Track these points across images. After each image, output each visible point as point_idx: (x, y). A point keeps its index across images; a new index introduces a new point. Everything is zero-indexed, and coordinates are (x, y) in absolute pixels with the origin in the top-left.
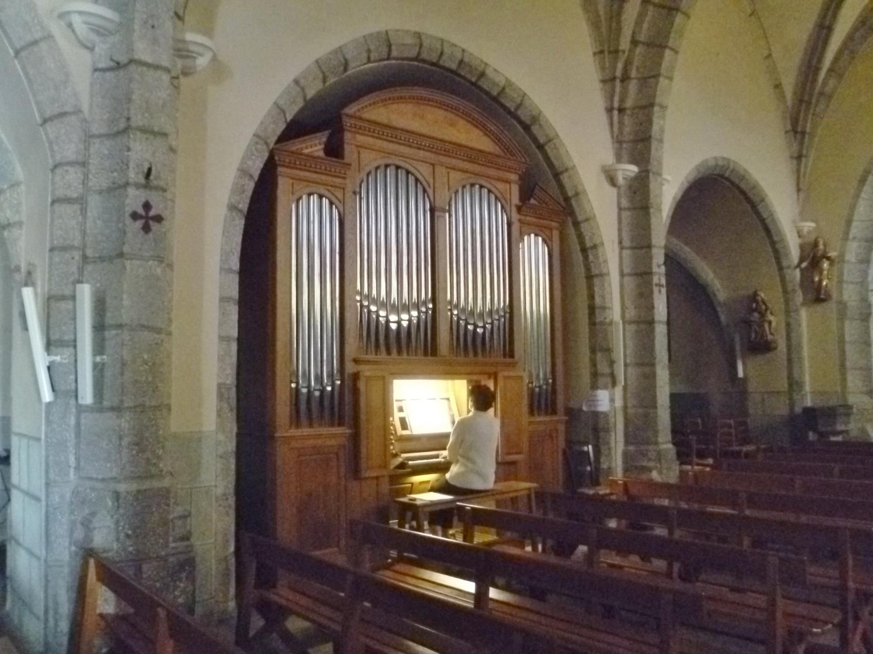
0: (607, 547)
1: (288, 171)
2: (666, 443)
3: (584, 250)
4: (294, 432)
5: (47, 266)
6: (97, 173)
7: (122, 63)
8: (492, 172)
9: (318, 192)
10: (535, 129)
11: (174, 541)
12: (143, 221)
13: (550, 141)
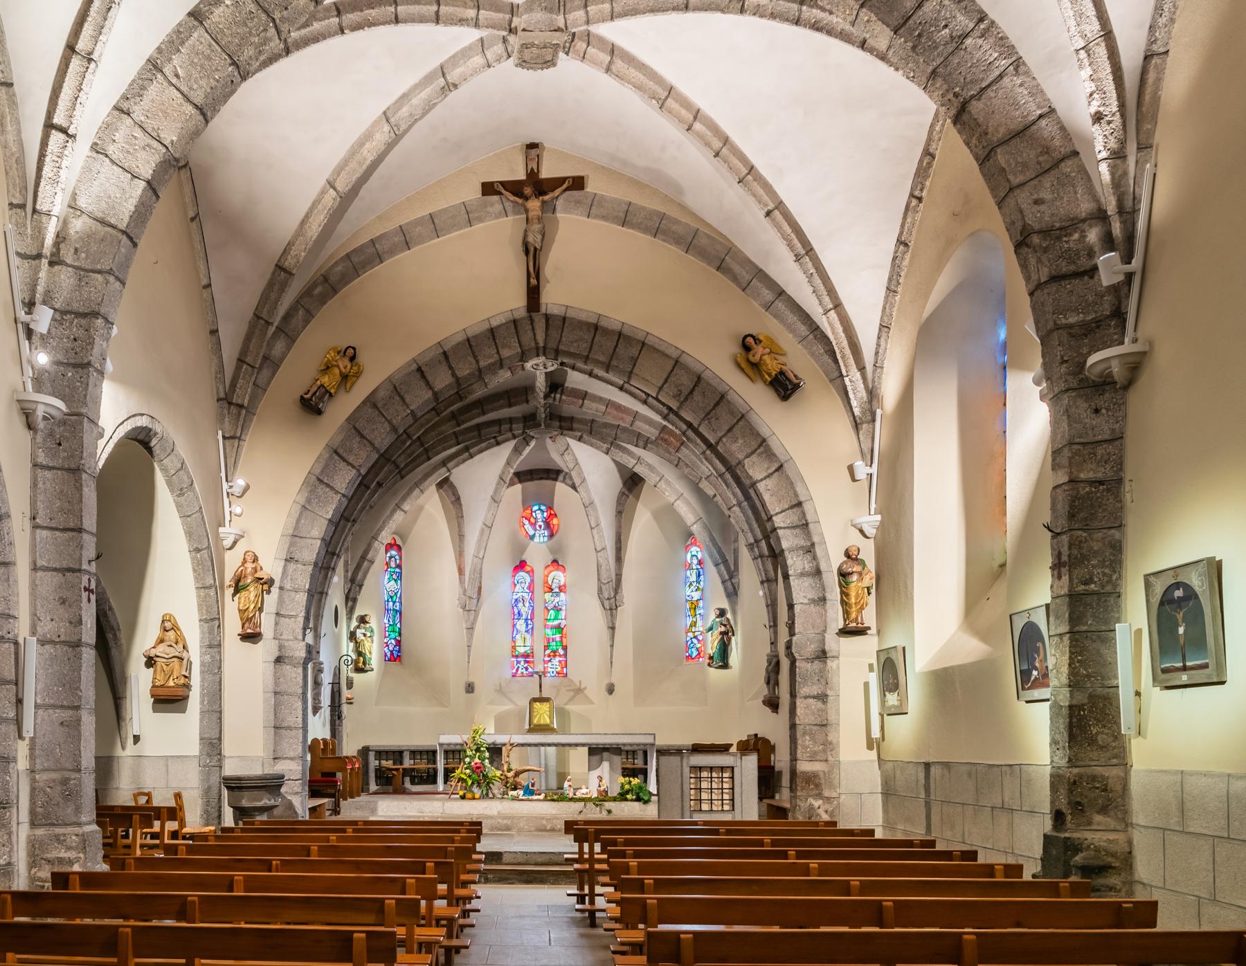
2: (89, 823)
5: (809, 357)
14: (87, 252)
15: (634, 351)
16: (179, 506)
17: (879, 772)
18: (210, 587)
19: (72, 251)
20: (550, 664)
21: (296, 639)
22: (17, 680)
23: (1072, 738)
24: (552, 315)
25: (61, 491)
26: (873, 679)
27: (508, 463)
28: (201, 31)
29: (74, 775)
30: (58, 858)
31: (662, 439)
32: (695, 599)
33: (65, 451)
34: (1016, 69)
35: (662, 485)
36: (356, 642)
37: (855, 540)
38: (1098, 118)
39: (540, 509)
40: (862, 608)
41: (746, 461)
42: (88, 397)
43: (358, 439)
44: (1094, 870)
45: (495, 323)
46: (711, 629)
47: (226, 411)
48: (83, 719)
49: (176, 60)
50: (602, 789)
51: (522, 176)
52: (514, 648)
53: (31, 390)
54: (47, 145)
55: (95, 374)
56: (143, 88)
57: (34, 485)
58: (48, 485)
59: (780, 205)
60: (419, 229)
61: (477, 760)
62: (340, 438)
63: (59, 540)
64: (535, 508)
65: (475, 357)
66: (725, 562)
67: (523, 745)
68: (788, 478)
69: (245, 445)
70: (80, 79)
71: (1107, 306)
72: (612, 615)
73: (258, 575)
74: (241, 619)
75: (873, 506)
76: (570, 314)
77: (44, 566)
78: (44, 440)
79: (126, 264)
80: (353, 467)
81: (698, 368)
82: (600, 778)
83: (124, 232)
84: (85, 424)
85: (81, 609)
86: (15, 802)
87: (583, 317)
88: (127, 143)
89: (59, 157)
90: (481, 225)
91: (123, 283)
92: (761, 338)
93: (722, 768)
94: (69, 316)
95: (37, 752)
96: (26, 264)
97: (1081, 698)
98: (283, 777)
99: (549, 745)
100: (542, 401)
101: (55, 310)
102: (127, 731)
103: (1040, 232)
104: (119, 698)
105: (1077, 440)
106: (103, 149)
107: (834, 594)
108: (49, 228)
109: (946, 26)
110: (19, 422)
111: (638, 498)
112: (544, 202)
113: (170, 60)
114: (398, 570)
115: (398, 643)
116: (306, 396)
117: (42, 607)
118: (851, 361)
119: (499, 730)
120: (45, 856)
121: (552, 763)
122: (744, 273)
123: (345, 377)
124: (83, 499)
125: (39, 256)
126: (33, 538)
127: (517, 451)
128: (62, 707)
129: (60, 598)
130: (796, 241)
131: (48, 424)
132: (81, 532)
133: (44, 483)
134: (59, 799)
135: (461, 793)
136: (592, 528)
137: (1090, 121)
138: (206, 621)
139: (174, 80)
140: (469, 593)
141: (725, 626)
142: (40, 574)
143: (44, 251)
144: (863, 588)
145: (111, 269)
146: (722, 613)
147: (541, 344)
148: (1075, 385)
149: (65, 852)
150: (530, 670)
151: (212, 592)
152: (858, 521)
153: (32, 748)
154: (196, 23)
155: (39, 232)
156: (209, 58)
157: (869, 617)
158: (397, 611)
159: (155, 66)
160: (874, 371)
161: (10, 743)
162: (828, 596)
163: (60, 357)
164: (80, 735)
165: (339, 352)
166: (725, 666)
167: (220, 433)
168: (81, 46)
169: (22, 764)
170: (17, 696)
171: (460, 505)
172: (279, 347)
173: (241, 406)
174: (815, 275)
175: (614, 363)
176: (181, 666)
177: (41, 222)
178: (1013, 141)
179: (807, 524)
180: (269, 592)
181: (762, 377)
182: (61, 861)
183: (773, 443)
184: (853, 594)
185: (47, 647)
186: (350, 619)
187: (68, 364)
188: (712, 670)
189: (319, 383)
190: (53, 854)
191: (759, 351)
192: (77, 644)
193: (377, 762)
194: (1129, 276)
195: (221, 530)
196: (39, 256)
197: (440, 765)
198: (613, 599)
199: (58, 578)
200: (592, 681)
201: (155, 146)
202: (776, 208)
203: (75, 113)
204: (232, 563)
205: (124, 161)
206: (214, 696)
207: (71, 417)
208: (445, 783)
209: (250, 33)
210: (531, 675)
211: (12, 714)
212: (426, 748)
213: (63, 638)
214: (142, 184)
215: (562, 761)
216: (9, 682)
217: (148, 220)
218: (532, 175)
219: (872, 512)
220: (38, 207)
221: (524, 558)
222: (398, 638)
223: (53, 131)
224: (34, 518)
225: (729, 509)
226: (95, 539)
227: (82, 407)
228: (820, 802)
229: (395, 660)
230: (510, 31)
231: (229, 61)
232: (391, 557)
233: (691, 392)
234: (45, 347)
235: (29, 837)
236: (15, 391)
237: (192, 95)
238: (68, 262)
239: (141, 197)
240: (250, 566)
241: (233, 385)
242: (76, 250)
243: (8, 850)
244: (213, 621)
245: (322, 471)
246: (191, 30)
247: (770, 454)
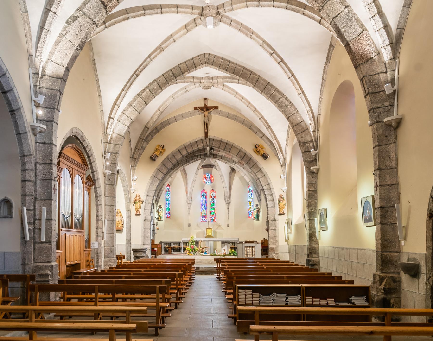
0: (49, 299)
3: (96, 196)
6: (39, 174)
7: (46, 143)
10: (91, 158)
14: (116, 141)
15: (230, 147)
16: (123, 184)
17: (288, 247)
18: (128, 203)
20: (211, 218)
21: (149, 215)
23: (309, 240)
24: (211, 138)
25: (110, 189)
26: (286, 225)
27: (200, 165)
28: (140, 98)
29: (113, 247)
31: (239, 162)
32: (251, 201)
33: (111, 181)
34: (297, 113)
35: (241, 172)
36: (158, 213)
37: (282, 193)
38: (310, 124)
39: (208, 175)
40: (283, 209)
41: (257, 173)
43: (164, 167)
44: (313, 265)
45: (197, 140)
46: (254, 210)
47: (132, 160)
49: (134, 103)
50: (225, 252)
51: (203, 106)
52: (201, 214)
56: (128, 109)
57: (105, 188)
59: (262, 117)
60: (179, 117)
61: (192, 245)
62: (160, 167)
64: (207, 175)
65: (192, 147)
66: (258, 192)
67: (204, 241)
68: (266, 178)
69: (136, 168)
71: (314, 158)
72: (228, 205)
73: (140, 200)
74: (136, 210)
75: (286, 185)
76: (215, 138)
80: (163, 173)
81: (245, 152)
82: (224, 250)
83: (123, 137)
87: (218, 139)
90: (194, 117)
92: (260, 145)
93: (252, 247)
97: (311, 232)
98: (147, 249)
99: (211, 241)
100: (209, 152)
103: (302, 143)
105: (310, 183)
107: (277, 205)
109: (284, 103)
110: (103, 175)
111: (235, 173)
112: (208, 112)
113: (133, 103)
114: (169, 192)
115: (169, 213)
116: (152, 157)
118: (280, 152)
119: (197, 237)
121: (212, 246)
122: (255, 130)
123: (161, 152)
126: (105, 199)
127: (202, 161)
128: (110, 233)
130: (266, 125)
135: (188, 254)
136: (222, 182)
137: (309, 124)
138: (128, 211)
139: (134, 107)
140: (189, 199)
141: (258, 209)
142: (106, 206)
144: (283, 204)
146: (257, 205)
147: (208, 145)
148: (309, 172)
150: (206, 220)
151: (129, 204)
152: (282, 188)
153: (105, 242)
154: (139, 96)
156: (141, 102)
157: (285, 211)
158: (169, 204)
159: (130, 105)
160: (285, 154)
162: (276, 206)
165: (159, 146)
166: (258, 220)
167: (131, 165)
169: (103, 245)
171: (186, 174)
172: (145, 144)
173: (136, 159)
174: (271, 132)
175: (225, 149)
176: (122, 222)
178: (297, 125)
179: (271, 189)
180: (142, 204)
181: (260, 154)
182: (110, 265)
183: (263, 170)
184: (281, 206)
186: (157, 206)
187: (112, 163)
188: (255, 221)
189: (155, 154)
190: (109, 264)
191: (259, 148)
193: (164, 246)
194: (394, 91)
195: (131, 189)
196: (107, 142)
197: (182, 246)
198: (228, 201)
200: (223, 224)
202: (262, 117)
204: (133, 197)
206: (129, 229)
208: (183, 251)
209: (149, 98)
210: (206, 221)
211: (102, 235)
212: (167, 242)
213: (110, 219)
214: (127, 127)
215: (215, 246)
218: (206, 106)
219: (286, 186)
220: (107, 133)
221: (204, 189)
222: (169, 211)
225: (257, 180)
228: (275, 255)
229: (168, 217)
230: (201, 83)
231: (145, 103)
232: (167, 189)
233: (244, 157)
235: (104, 260)
237: (137, 110)
240: (138, 198)
241: (134, 153)
244: (129, 211)
245: (155, 175)
246: (137, 98)
247: (262, 172)
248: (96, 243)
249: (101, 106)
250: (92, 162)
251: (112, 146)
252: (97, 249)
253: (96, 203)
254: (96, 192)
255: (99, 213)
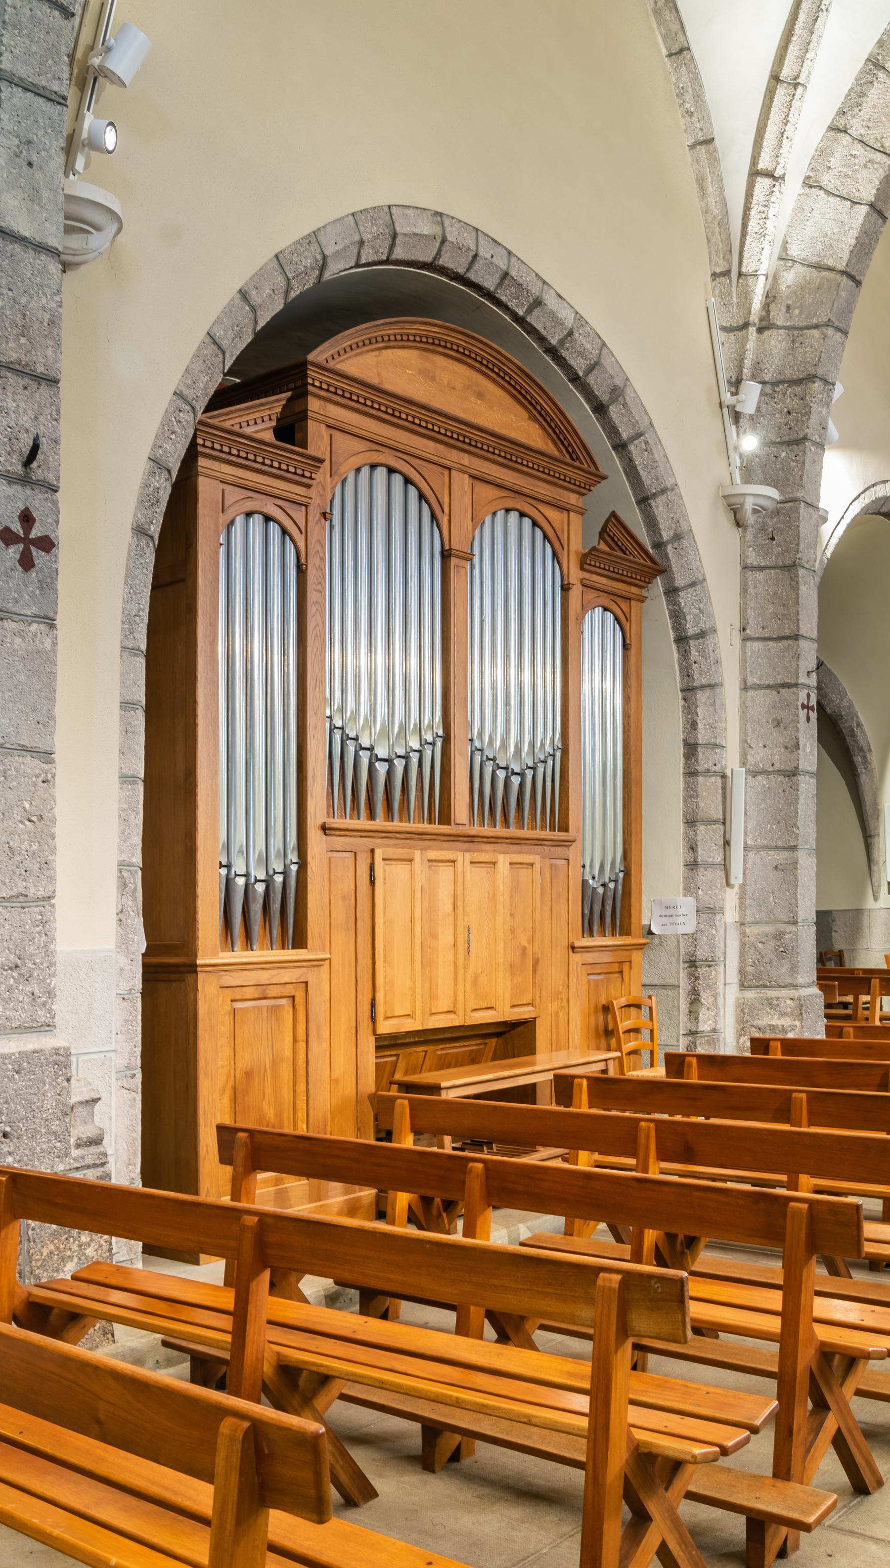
1: (215, 465)
4: (226, 957)
8: (543, 490)
9: (265, 510)
11: (78, 1146)
12: (21, 546)
13: (639, 435)
14: (801, 307)
19: (784, 309)
22: (724, 819)
30: (770, 1026)
33: (778, 545)
42: (805, 477)
48: (800, 861)
53: (739, 482)
54: (752, 196)
55: (813, 448)
56: (862, 95)
57: (744, 590)
58: (760, 588)
63: (773, 652)
70: (786, 110)
77: (755, 684)
78: (755, 537)
79: (847, 310)
83: (843, 273)
84: (802, 511)
85: (797, 730)
86: (722, 959)
88: (844, 166)
89: (765, 206)
91: (845, 333)
94: (781, 387)
95: (748, 901)
96: (733, 338)
101: (763, 383)
102: (880, 877)
104: (870, 836)
106: (817, 182)
108: (756, 291)
110: (725, 520)
117: (753, 731)
120: (755, 1023)
124: (800, 600)
125: (746, 325)
128: (777, 848)
129: (774, 720)
131: (760, 517)
132: (797, 639)
133: (755, 587)
134: (772, 956)
142: (751, 693)
143: (751, 319)
145: (829, 320)
149: (779, 1019)
153: (742, 898)
155: (746, 298)
161: (717, 891)
163: (773, 437)
164: (796, 880)
168: (786, 73)
169: (731, 915)
170: (724, 837)
177: (747, 285)
185: (759, 778)
192: (793, 773)
199: (772, 695)
201: (878, 160)
203: (781, 151)
205: (842, 187)
207: (786, 505)
211: (719, 858)
213: (777, 767)
214: (864, 209)
216: (715, 822)
217: (874, 249)
220: (744, 270)
223: (759, 179)
224: (744, 629)
226: (816, 645)
227: (798, 490)
234: (754, 429)
235: (738, 999)
236: (721, 486)
238: (779, 324)
239: (863, 225)
242: (788, 307)
243: (713, 1014)
248: (687, 905)
249: (691, 114)
250: (625, 436)
251: (777, 341)
252: (693, 938)
253: (682, 679)
254: (677, 616)
255: (703, 735)
